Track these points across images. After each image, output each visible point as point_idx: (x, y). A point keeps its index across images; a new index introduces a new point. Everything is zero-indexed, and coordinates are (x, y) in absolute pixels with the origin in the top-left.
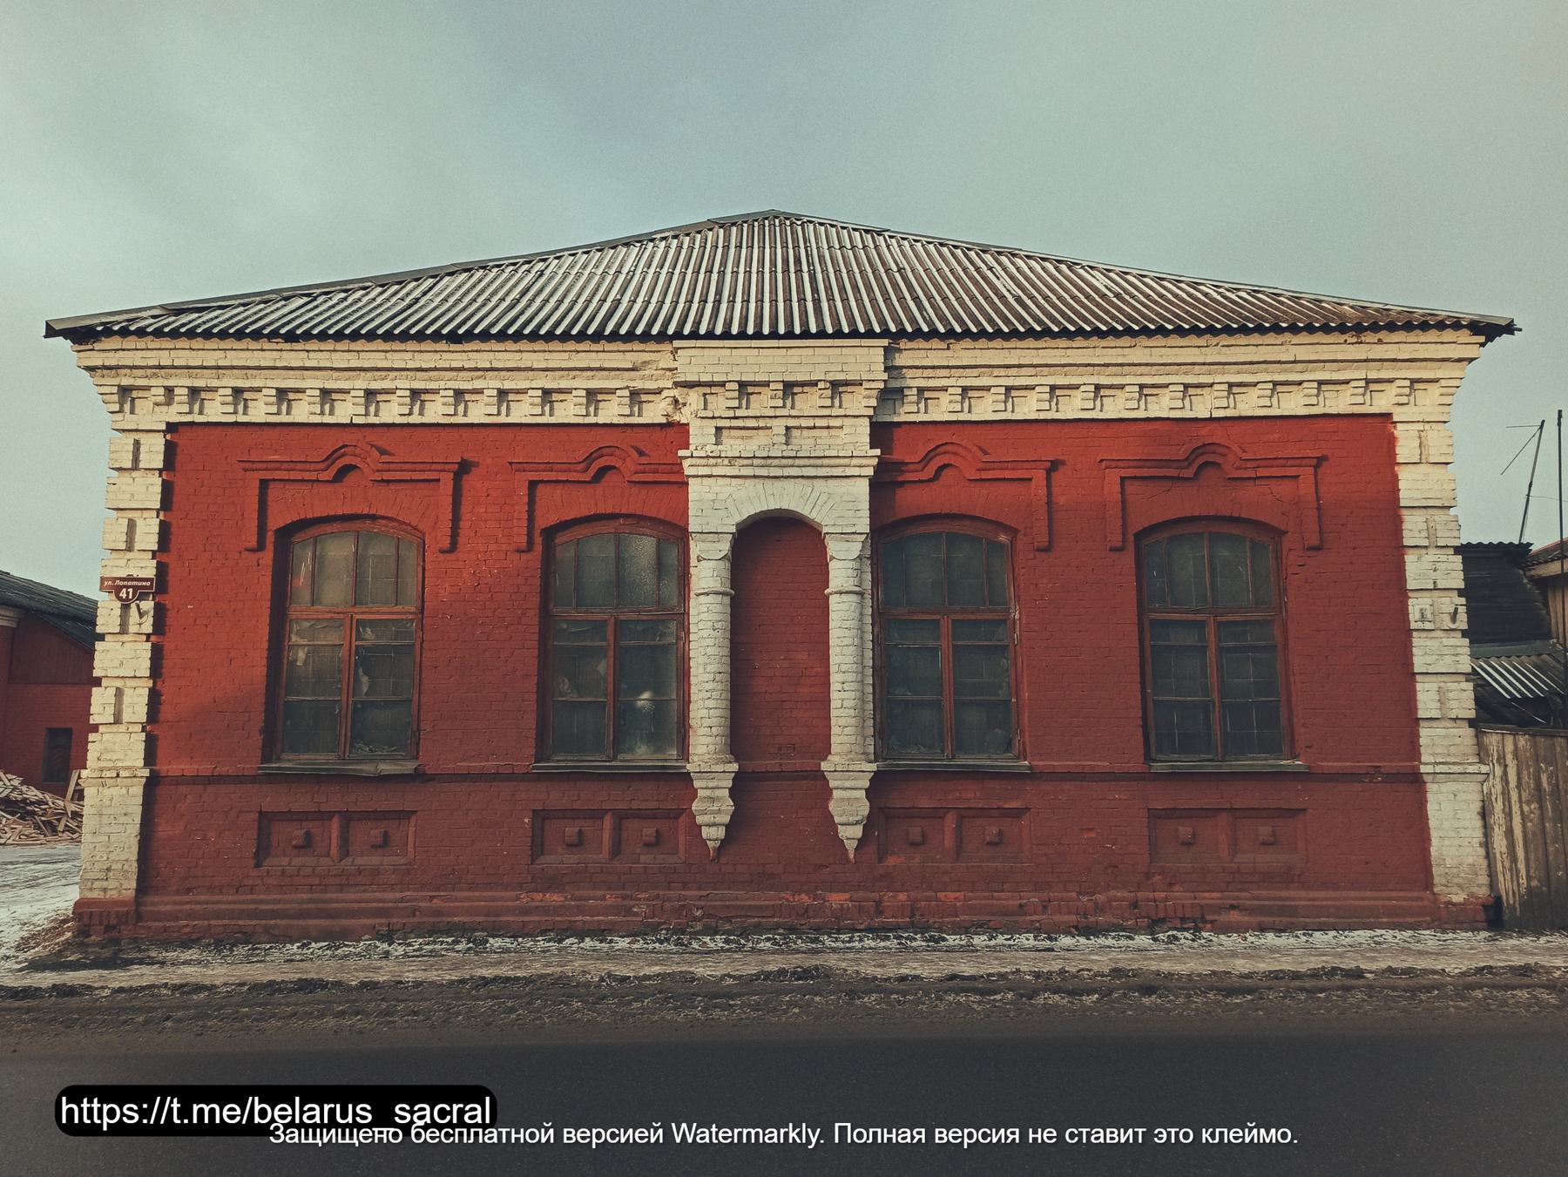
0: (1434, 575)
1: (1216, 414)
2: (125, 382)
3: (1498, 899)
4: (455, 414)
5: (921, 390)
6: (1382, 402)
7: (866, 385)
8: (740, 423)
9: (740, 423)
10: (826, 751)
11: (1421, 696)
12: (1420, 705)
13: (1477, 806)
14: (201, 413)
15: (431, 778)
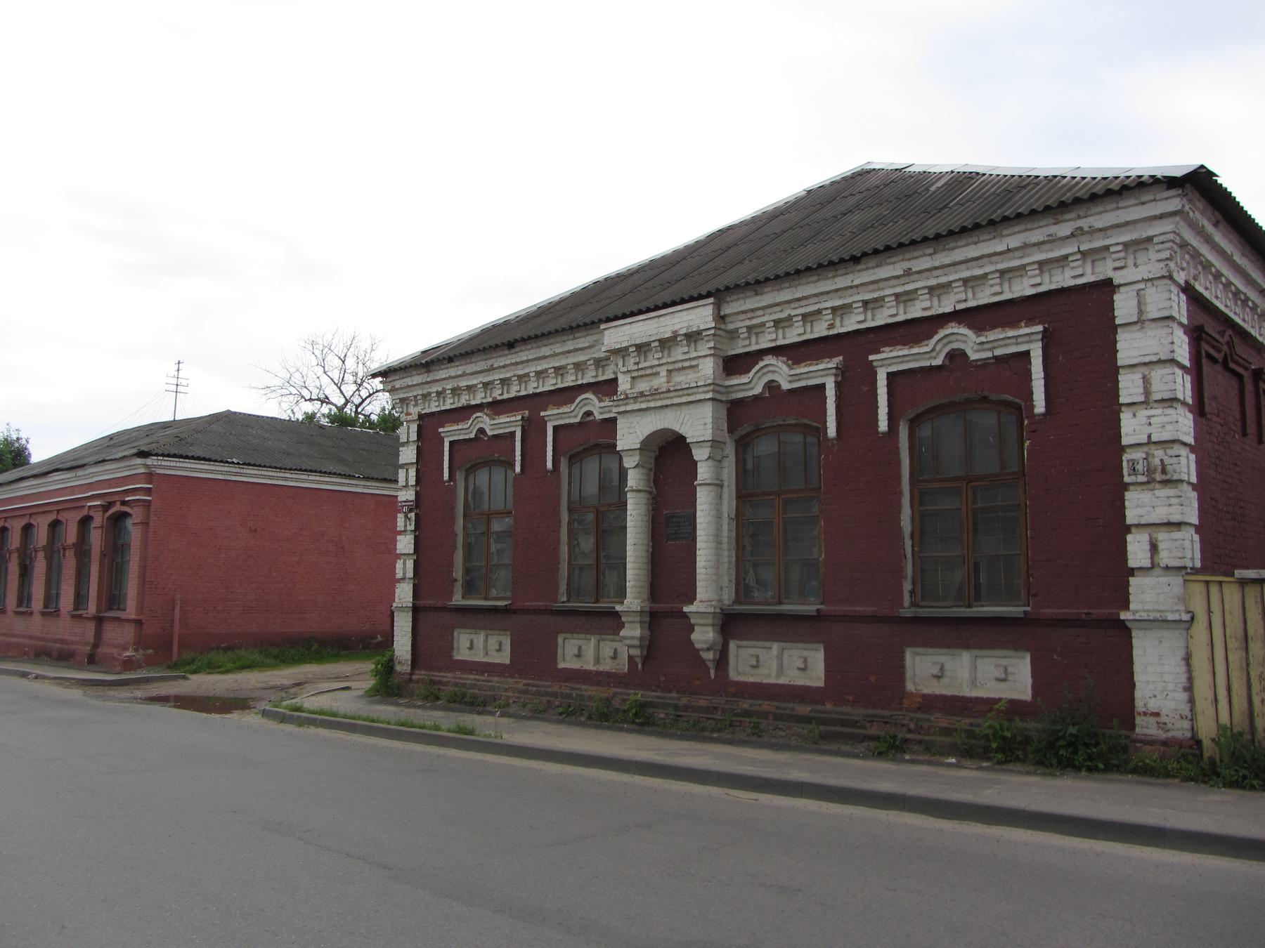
0: (1149, 430)
1: (960, 307)
2: (402, 396)
3: (1199, 743)
4: (864, 321)
5: (749, 328)
6: (1104, 270)
7: (1156, 240)
8: (643, 373)
9: (643, 373)
10: (691, 598)
11: (1130, 548)
12: (1130, 556)
13: (1181, 653)
14: (757, 343)
15: (515, 612)
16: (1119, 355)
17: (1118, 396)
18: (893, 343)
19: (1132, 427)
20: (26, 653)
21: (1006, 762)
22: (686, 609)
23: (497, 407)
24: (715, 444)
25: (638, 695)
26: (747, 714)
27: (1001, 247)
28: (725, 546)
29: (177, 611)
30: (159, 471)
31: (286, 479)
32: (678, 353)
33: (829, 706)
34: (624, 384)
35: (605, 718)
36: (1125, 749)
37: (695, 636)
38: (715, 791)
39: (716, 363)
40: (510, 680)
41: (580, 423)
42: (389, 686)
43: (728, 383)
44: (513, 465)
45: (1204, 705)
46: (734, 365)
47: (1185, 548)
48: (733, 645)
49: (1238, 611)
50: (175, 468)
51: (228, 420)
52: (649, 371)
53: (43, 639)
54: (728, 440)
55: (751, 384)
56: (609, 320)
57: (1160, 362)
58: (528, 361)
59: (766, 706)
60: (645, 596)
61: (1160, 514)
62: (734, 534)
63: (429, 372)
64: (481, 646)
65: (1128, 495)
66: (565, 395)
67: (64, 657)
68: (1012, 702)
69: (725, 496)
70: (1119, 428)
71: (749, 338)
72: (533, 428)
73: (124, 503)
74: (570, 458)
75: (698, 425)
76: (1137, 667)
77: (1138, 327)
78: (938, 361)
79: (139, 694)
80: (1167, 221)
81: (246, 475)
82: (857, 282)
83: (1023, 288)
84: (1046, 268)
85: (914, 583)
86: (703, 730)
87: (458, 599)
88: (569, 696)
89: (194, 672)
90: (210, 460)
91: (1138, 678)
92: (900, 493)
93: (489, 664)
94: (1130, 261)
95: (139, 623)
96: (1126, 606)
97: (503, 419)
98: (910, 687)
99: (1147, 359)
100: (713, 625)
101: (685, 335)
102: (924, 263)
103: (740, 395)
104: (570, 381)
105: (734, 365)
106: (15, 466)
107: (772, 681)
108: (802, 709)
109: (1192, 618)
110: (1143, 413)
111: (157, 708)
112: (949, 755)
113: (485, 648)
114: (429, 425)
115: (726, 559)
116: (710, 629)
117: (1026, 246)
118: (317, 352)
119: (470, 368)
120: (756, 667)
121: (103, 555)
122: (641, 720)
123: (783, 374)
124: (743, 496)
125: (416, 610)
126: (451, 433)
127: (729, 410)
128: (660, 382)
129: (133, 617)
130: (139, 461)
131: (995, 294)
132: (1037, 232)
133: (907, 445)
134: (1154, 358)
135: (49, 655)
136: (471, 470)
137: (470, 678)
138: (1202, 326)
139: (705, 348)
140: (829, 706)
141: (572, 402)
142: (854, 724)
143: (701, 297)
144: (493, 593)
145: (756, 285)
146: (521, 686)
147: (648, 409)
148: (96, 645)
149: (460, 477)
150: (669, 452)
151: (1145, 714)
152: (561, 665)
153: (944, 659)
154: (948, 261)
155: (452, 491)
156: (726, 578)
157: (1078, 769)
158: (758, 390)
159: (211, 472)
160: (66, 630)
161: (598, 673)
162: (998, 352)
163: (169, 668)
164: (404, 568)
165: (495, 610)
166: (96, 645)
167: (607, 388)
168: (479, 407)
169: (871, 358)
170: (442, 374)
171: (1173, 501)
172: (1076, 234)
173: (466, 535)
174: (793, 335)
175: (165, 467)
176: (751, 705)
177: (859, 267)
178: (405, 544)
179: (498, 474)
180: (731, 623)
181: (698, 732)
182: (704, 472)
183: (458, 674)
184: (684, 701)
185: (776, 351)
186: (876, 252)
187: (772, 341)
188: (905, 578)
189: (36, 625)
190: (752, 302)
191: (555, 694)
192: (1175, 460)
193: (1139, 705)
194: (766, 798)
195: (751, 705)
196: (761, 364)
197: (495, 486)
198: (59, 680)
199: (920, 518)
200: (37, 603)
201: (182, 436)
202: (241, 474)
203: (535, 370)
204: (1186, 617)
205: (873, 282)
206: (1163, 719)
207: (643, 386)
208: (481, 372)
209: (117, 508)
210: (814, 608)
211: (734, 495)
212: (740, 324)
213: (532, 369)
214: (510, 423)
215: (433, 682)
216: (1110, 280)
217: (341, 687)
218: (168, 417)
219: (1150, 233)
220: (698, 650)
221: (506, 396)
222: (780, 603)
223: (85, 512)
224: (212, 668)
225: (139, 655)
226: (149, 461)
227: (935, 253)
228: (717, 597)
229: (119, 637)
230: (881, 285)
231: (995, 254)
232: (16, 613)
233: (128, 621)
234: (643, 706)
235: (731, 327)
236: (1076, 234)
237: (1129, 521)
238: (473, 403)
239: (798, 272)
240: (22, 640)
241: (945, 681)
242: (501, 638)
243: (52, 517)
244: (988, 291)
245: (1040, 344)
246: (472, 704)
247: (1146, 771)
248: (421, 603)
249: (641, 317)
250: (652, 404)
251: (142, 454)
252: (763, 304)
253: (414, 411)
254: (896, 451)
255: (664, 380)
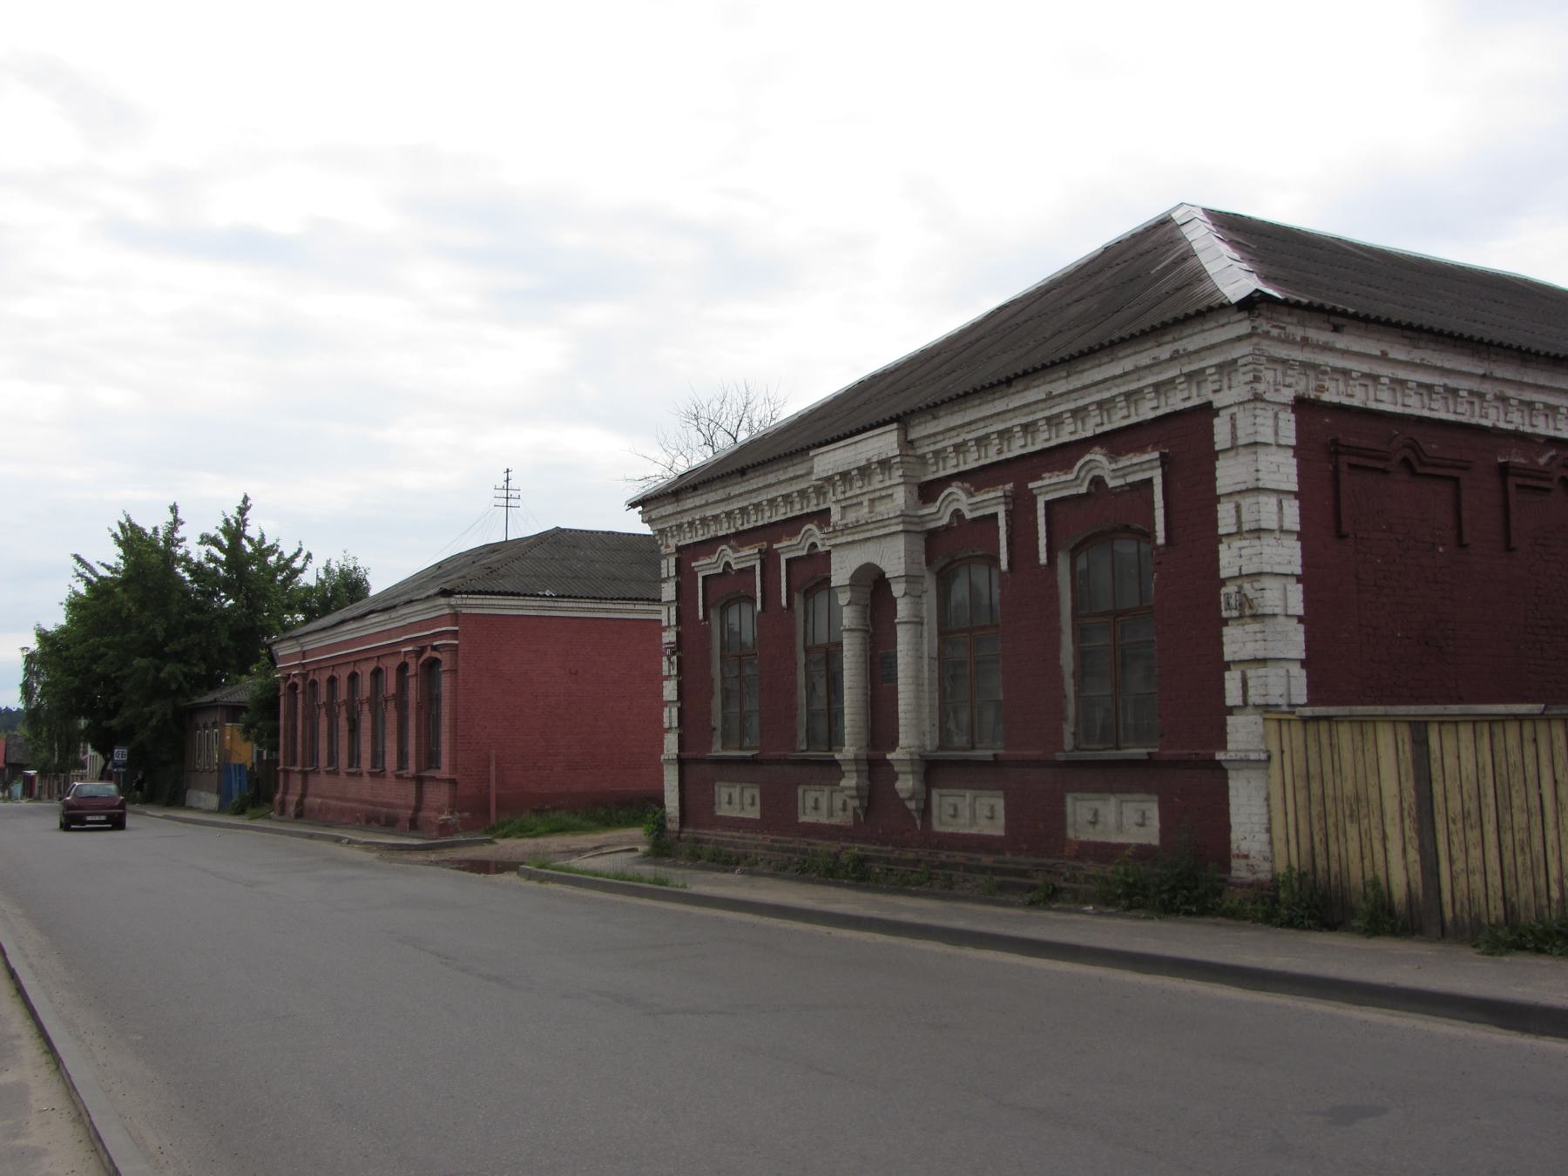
1: (1099, 430)
10: (894, 744)
13: (1263, 793)
16: (1218, 483)
17: (1216, 527)
18: (1051, 469)
19: (1230, 559)
20: (358, 819)
21: (1130, 908)
22: (889, 756)
23: (1116, 442)
24: (910, 578)
25: (856, 849)
26: (943, 865)
27: (1118, 371)
28: (926, 688)
29: (493, 768)
30: (465, 611)
31: (608, 611)
32: (877, 481)
33: (1008, 856)
34: (835, 516)
35: (832, 874)
36: (1219, 893)
37: (899, 785)
38: (881, 938)
39: (908, 492)
40: (760, 837)
41: (1088, 495)
42: (662, 849)
43: (926, 511)
44: (997, 560)
45: (1279, 846)
46: (928, 491)
47: (1288, 684)
48: (935, 793)
49: (1302, 749)
50: (482, 607)
51: (558, 541)
52: (855, 501)
53: (372, 803)
54: (927, 574)
55: (939, 515)
56: (821, 445)
57: (1248, 490)
58: (759, 489)
59: (960, 857)
60: (864, 744)
61: (1249, 651)
62: (936, 675)
63: (678, 501)
64: (737, 801)
65: (1226, 630)
66: (1063, 456)
67: (389, 823)
68: (1140, 847)
69: (925, 634)
70: (1217, 560)
71: (936, 464)
72: (1020, 506)
73: (435, 648)
74: (806, 592)
75: (893, 558)
76: (1233, 809)
77: (1232, 453)
78: (1083, 490)
79: (433, 857)
80: (1245, 343)
81: (561, 609)
82: (1011, 406)
83: (1146, 411)
84: (1162, 390)
85: (1076, 725)
86: (907, 883)
87: (717, 751)
88: (805, 852)
89: (505, 836)
90: (518, 594)
91: (1234, 820)
92: (1059, 630)
93: (743, 820)
94: (1225, 381)
95: (453, 782)
96: (1223, 745)
97: (746, 551)
98: (1071, 834)
99: (1238, 488)
100: (913, 772)
101: (879, 462)
102: (1060, 387)
103: (933, 525)
104: (797, 511)
105: (928, 491)
106: (352, 601)
107: (966, 831)
108: (987, 860)
109: (1269, 758)
110: (1237, 544)
111: (432, 869)
112: (1086, 903)
113: (742, 804)
114: (685, 555)
115: (927, 702)
116: (910, 777)
117: (1137, 369)
118: (703, 428)
119: (712, 497)
120: (954, 816)
121: (419, 707)
122: (860, 875)
123: (959, 500)
124: (944, 633)
125: (681, 762)
126: (706, 566)
127: (927, 541)
128: (863, 513)
129: (447, 776)
130: (442, 601)
131: (1125, 418)
132: (1145, 354)
133: (1068, 578)
134: (1243, 487)
135: (378, 821)
136: (724, 610)
137: (728, 835)
138: (1335, 442)
139: (897, 475)
140: (1008, 856)
141: (935, 500)
142: (1024, 874)
143: (885, 423)
144: (747, 742)
145: (932, 409)
146: (768, 843)
147: (853, 542)
148: (417, 809)
149: (715, 616)
150: (873, 584)
151: (1238, 856)
152: (802, 819)
153: (1097, 804)
154: (1099, 377)
155: (707, 631)
156: (927, 722)
157: (1176, 912)
158: (945, 520)
159: (522, 607)
160: (399, 795)
161: (831, 826)
162: (1130, 479)
163: (486, 832)
164: (670, 716)
165: (743, 761)
166: (417, 809)
167: (822, 516)
168: (725, 539)
169: (1031, 485)
170: (689, 503)
171: (1259, 636)
172: (1175, 357)
173: (723, 679)
174: (972, 461)
175: (470, 606)
176: (861, 849)
177: (1012, 390)
178: (670, 690)
179: (746, 610)
180: (933, 770)
181: (901, 886)
182: (903, 609)
183: (719, 832)
184: (896, 854)
185: (961, 476)
186: (1026, 373)
187: (1125, 418)
188: (1064, 719)
189: (365, 788)
190: (931, 427)
191: (794, 851)
192: (1259, 594)
193: (1234, 846)
194: (970, 952)
195: (861, 849)
196: (946, 492)
197: (744, 621)
198: (368, 846)
199: (1081, 655)
200: (366, 765)
201: (494, 566)
202: (556, 609)
203: (765, 499)
204: (1263, 756)
205: (1025, 406)
206: (1251, 861)
207: (851, 517)
208: (722, 500)
209: (428, 654)
210: (990, 753)
211: (935, 632)
212: (926, 449)
213: (763, 497)
214: (745, 557)
215: (697, 841)
216: (1210, 403)
217: (617, 850)
218: (497, 537)
219: (1235, 354)
220: (903, 800)
221: (746, 526)
222: (973, 748)
223: (401, 659)
224: (525, 831)
225: (454, 819)
226: (453, 601)
227: (1069, 376)
228: (917, 743)
229: (437, 796)
230: (1033, 408)
231: (1115, 377)
232: (349, 774)
233: (442, 780)
234: (861, 861)
235: (920, 452)
236: (1175, 357)
237: (1227, 658)
238: (720, 534)
239: (1035, 370)
240: (354, 805)
241: (1099, 827)
242: (1144, 806)
243: (372, 666)
244: (1180, 396)
245: (1160, 471)
246: (727, 863)
247: (1233, 915)
248: (685, 755)
249: (842, 443)
250: (856, 537)
251: (445, 593)
252: (940, 429)
253: (673, 542)
254: (1054, 586)
255: (866, 510)
